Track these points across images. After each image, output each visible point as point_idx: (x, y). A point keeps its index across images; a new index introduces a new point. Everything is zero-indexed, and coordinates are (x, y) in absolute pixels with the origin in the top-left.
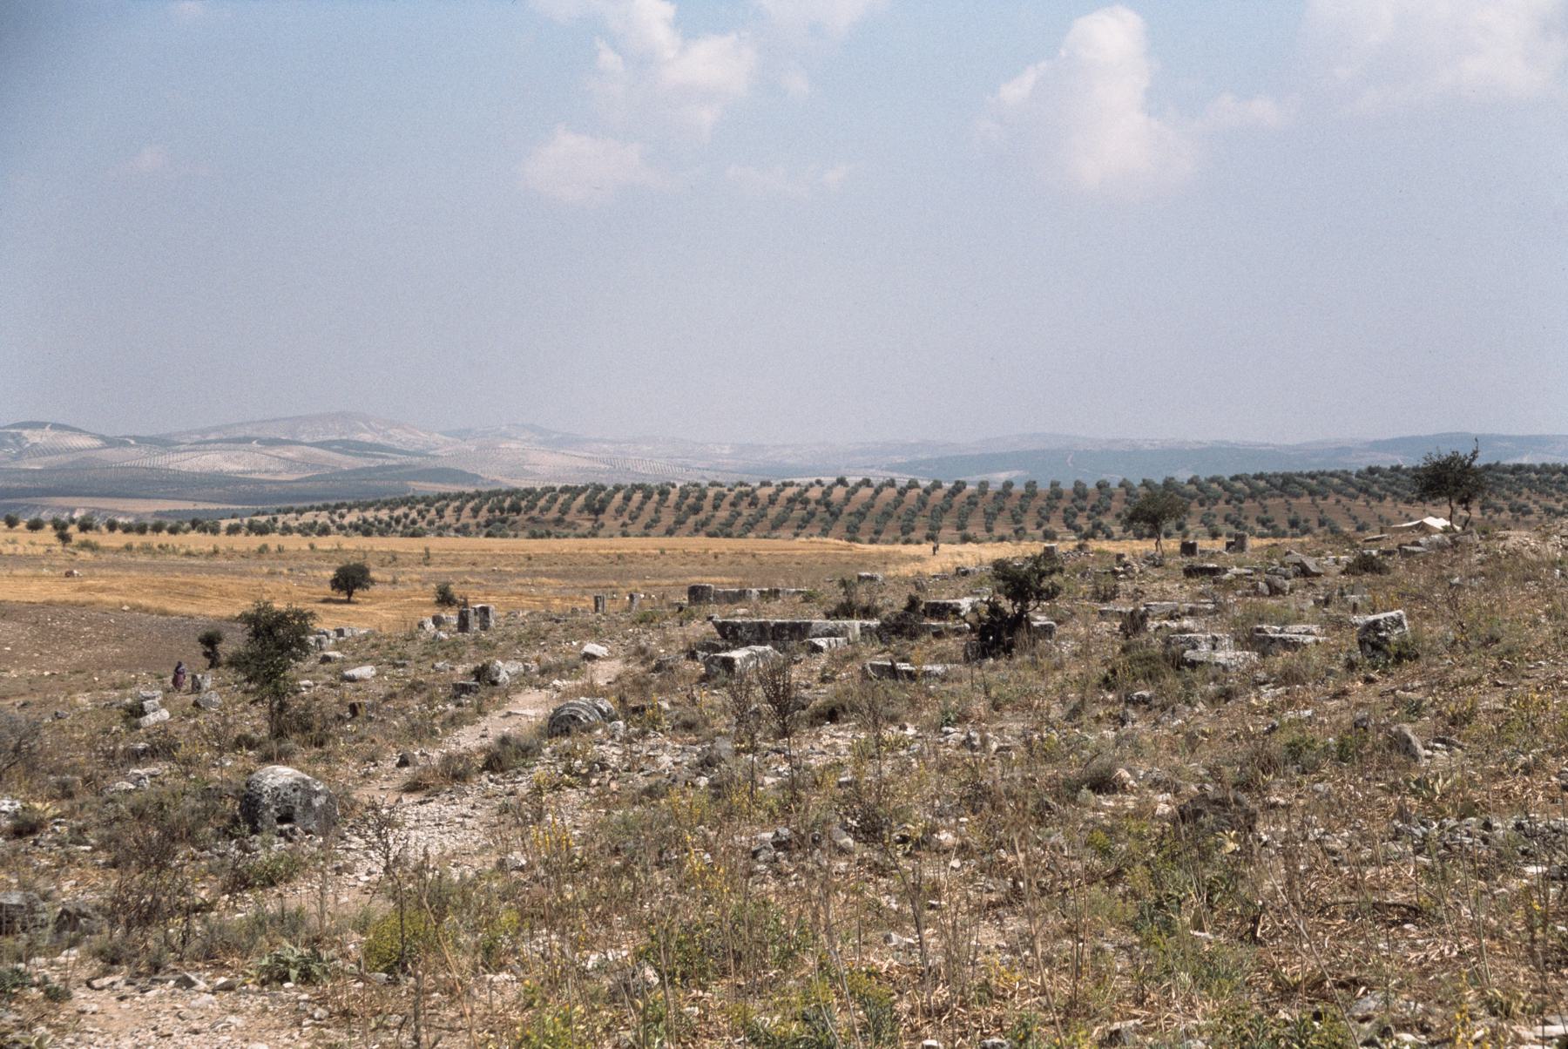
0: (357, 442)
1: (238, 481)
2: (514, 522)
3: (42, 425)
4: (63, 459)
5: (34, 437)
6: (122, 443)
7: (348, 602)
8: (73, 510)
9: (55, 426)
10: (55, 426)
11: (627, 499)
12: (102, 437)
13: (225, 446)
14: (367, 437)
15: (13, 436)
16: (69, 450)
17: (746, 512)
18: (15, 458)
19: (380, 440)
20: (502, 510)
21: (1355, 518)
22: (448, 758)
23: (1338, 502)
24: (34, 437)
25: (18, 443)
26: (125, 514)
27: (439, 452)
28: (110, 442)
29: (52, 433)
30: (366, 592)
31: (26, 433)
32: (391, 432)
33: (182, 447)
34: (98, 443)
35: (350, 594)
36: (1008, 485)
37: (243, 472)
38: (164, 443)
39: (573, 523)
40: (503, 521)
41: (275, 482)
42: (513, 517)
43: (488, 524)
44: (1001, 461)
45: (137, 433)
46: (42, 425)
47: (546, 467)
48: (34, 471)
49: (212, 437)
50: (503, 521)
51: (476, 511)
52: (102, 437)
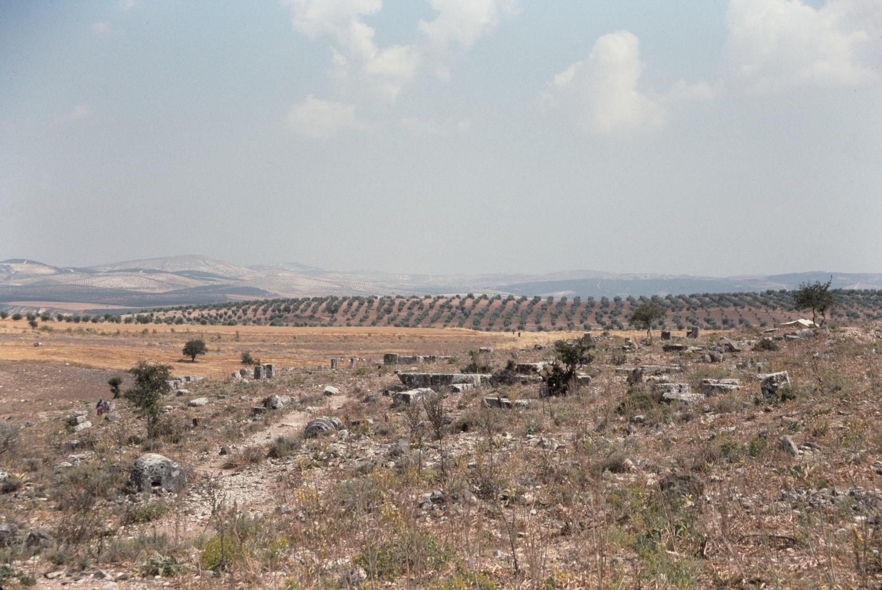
1: (131, 293)
2: (286, 318)
3: (21, 261)
4: (29, 281)
5: (17, 268)
6: (66, 271)
7: (193, 362)
8: (38, 309)
9: (29, 262)
10: (29, 262)
12: (55, 268)
13: (125, 273)
15: (5, 267)
16: (37, 275)
17: (417, 313)
19: (211, 271)
20: (279, 311)
23: (750, 310)
24: (17, 268)
25: (8, 271)
27: (245, 278)
28: (60, 271)
29: (28, 265)
31: (13, 265)
32: (218, 266)
33: (100, 274)
34: (53, 271)
35: (193, 357)
38: (90, 272)
39: (319, 318)
40: (280, 317)
42: (286, 314)
46: (21, 261)
47: (305, 287)
49: (117, 268)
51: (265, 311)
52: (55, 268)
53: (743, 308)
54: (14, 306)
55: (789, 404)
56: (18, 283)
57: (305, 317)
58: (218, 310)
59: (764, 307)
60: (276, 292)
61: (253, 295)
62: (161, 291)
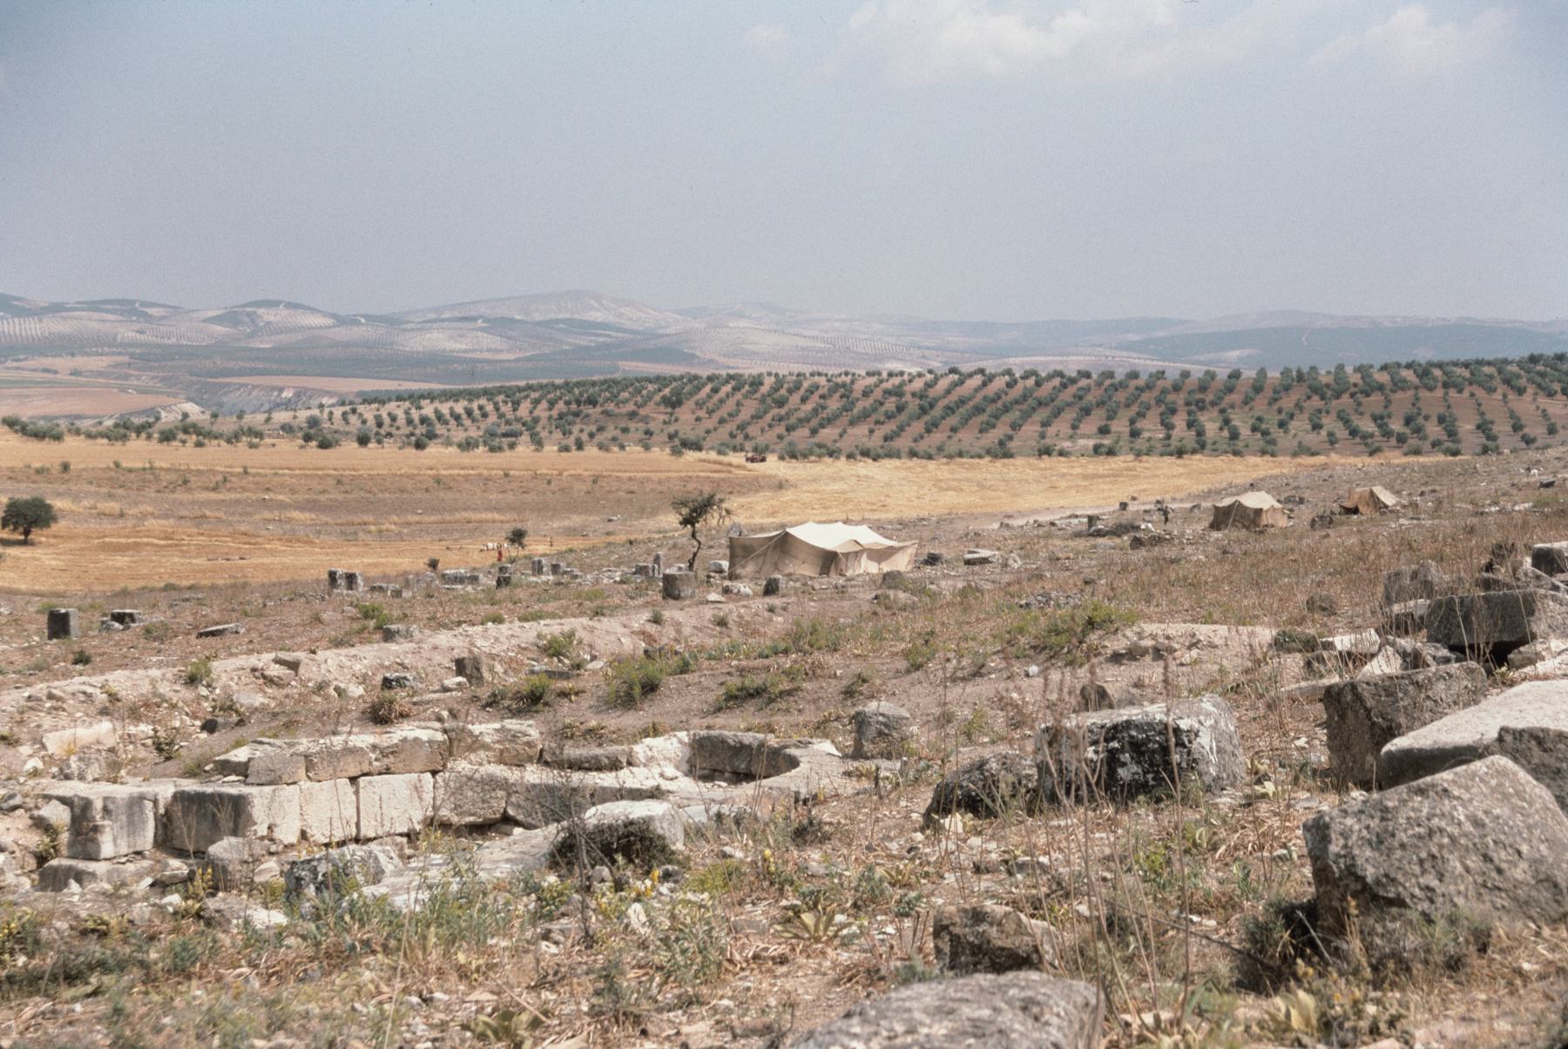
0: (581, 321)
4: (284, 338)
5: (268, 316)
6: (352, 321)
7: (25, 543)
8: (281, 390)
9: (289, 305)
10: (289, 305)
11: (715, 390)
12: (333, 316)
13: (459, 325)
14: (598, 316)
15: (248, 315)
16: (294, 330)
17: (834, 404)
18: (251, 336)
20: (578, 403)
21: (1482, 414)
22: (858, 714)
23: (1472, 395)
24: (268, 316)
25: (253, 321)
26: (329, 394)
27: (668, 331)
28: (341, 321)
29: (286, 312)
30: (45, 531)
31: (261, 311)
33: (409, 326)
34: (330, 321)
35: (27, 533)
36: (1186, 375)
37: (465, 351)
38: (393, 321)
40: (577, 415)
41: (489, 362)
42: (589, 410)
43: (561, 416)
44: (1222, 340)
45: (371, 312)
47: (763, 345)
48: (264, 350)
49: (447, 315)
50: (577, 415)
51: (552, 404)
52: (333, 316)
53: (1460, 391)
54: (242, 385)
55: (937, 642)
56: (265, 344)
57: (621, 415)
58: (470, 401)
59: (1501, 389)
60: (713, 356)
61: (657, 361)
62: (512, 357)
